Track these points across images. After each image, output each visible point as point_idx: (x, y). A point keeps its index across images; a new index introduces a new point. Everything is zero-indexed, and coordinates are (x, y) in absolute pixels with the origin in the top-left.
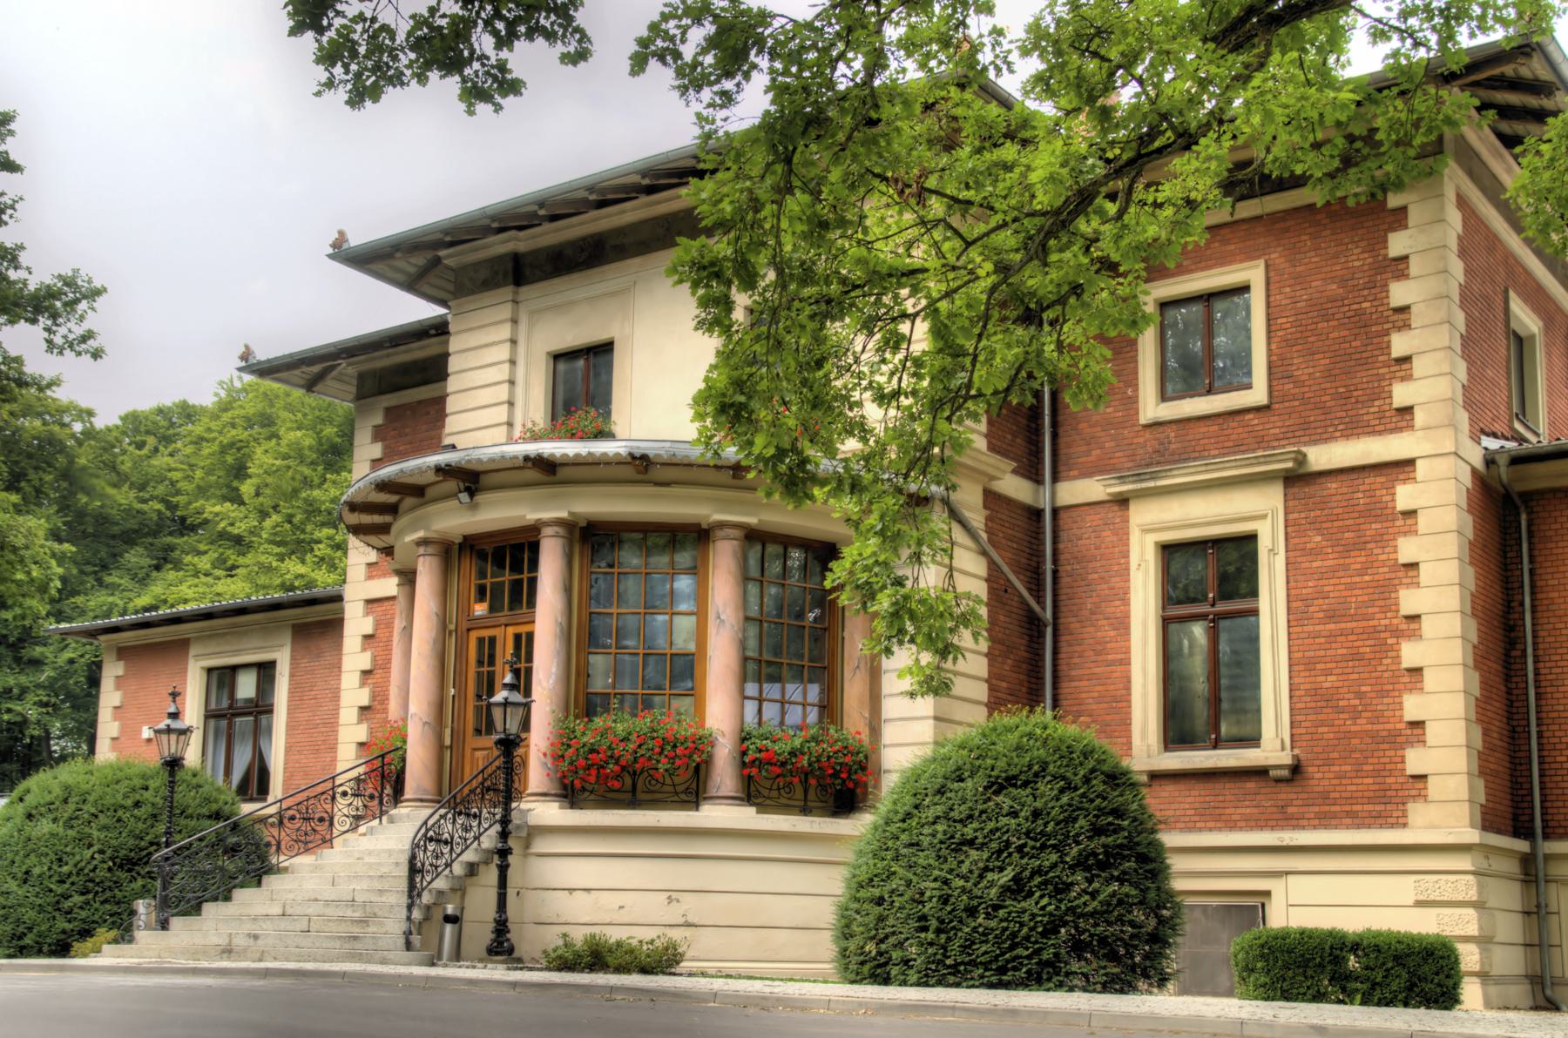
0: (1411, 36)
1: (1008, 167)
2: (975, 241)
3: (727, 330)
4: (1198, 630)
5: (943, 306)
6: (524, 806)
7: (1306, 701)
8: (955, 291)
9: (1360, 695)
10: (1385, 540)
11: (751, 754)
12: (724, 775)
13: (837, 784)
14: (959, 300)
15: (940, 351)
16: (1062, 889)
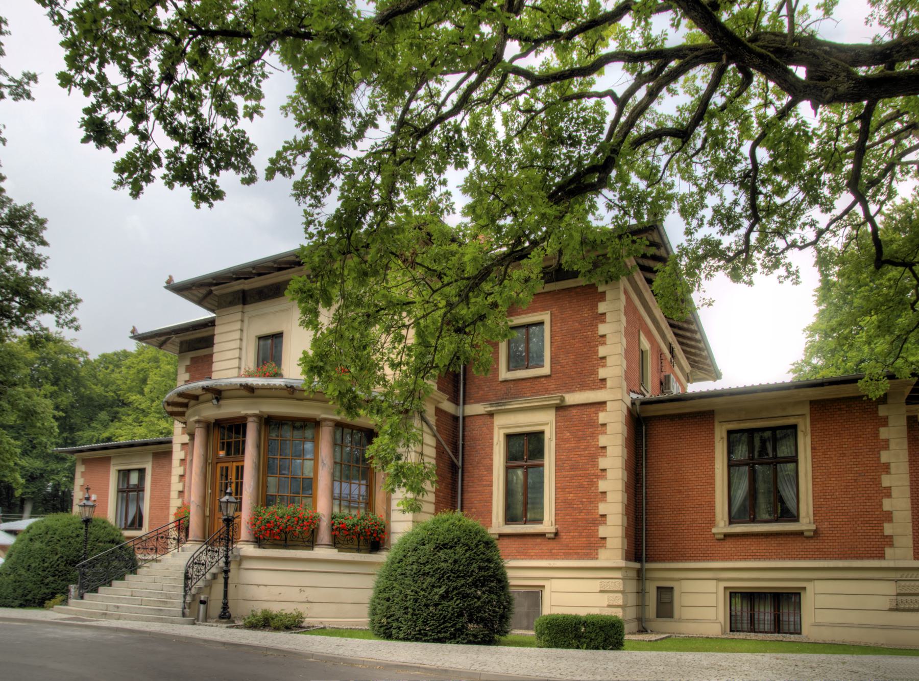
0: (623, 209)
1: (453, 254)
2: (437, 290)
3: (316, 327)
4: (520, 472)
5: (422, 321)
6: (239, 546)
7: (562, 506)
8: (428, 314)
9: (582, 503)
10: (594, 436)
11: (336, 525)
12: (324, 535)
13: (372, 539)
14: (429, 320)
15: (420, 344)
16: (465, 596)
